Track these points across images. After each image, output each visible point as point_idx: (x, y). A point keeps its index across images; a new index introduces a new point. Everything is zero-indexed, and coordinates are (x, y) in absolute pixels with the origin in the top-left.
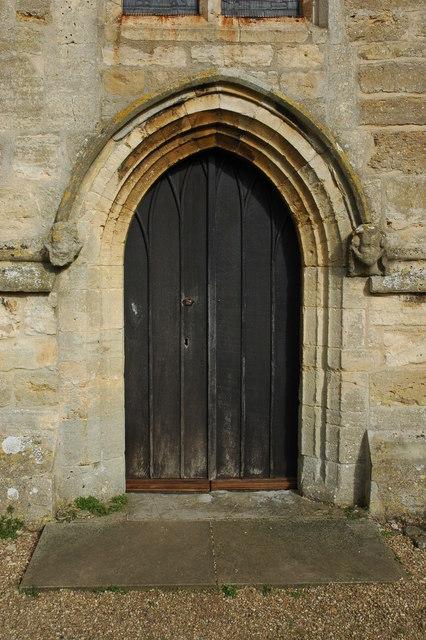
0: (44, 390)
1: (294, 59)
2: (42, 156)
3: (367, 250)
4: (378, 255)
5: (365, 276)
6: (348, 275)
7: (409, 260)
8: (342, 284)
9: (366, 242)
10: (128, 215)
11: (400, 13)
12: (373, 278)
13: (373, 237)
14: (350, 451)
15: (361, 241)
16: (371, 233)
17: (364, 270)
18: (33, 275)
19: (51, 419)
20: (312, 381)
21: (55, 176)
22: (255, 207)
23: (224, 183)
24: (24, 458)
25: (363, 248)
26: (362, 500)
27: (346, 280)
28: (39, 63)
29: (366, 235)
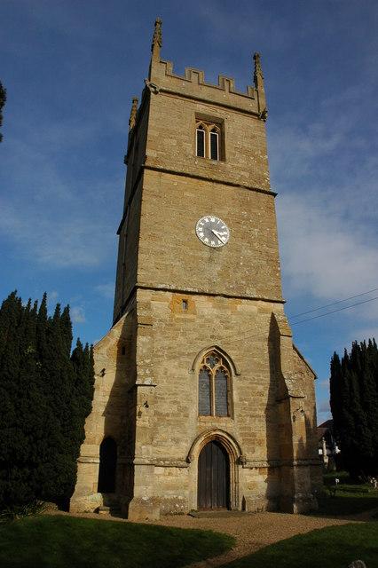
0: (186, 486)
1: (229, 425)
2: (186, 441)
10: (298, 460)
11: (296, 524)
14: (241, 499)
17: (242, 463)
18: (185, 464)
19: (187, 492)
20: (232, 486)
21: (189, 445)
22: (220, 451)
23: (214, 446)
24: (184, 500)
26: (244, 509)
28: (186, 424)
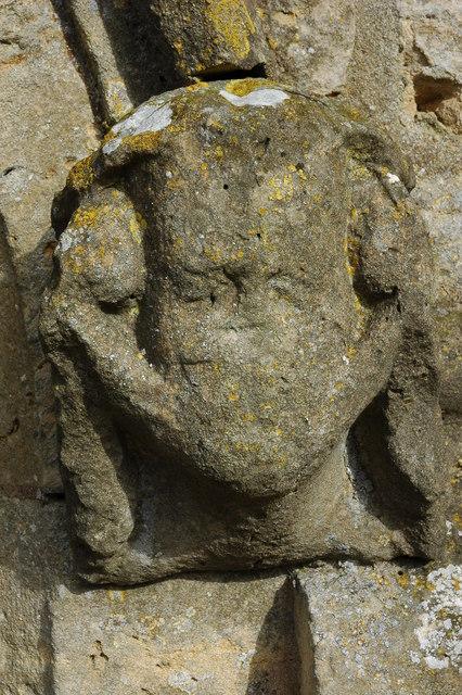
3: (214, 331)
4: (342, 381)
5: (253, 570)
6: (86, 569)
7: (197, 300)
8: (47, 646)
9: (191, 246)
12: (304, 577)
13: (279, 185)
15: (154, 241)
16: (257, 144)
25: (179, 319)
27: (82, 619)
29: (195, 180)
